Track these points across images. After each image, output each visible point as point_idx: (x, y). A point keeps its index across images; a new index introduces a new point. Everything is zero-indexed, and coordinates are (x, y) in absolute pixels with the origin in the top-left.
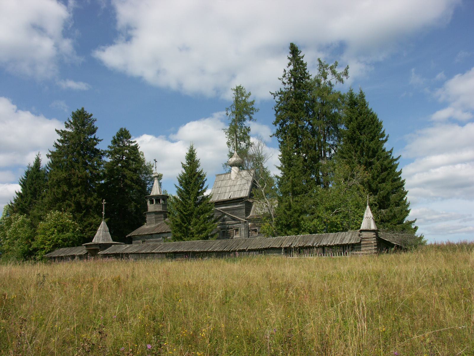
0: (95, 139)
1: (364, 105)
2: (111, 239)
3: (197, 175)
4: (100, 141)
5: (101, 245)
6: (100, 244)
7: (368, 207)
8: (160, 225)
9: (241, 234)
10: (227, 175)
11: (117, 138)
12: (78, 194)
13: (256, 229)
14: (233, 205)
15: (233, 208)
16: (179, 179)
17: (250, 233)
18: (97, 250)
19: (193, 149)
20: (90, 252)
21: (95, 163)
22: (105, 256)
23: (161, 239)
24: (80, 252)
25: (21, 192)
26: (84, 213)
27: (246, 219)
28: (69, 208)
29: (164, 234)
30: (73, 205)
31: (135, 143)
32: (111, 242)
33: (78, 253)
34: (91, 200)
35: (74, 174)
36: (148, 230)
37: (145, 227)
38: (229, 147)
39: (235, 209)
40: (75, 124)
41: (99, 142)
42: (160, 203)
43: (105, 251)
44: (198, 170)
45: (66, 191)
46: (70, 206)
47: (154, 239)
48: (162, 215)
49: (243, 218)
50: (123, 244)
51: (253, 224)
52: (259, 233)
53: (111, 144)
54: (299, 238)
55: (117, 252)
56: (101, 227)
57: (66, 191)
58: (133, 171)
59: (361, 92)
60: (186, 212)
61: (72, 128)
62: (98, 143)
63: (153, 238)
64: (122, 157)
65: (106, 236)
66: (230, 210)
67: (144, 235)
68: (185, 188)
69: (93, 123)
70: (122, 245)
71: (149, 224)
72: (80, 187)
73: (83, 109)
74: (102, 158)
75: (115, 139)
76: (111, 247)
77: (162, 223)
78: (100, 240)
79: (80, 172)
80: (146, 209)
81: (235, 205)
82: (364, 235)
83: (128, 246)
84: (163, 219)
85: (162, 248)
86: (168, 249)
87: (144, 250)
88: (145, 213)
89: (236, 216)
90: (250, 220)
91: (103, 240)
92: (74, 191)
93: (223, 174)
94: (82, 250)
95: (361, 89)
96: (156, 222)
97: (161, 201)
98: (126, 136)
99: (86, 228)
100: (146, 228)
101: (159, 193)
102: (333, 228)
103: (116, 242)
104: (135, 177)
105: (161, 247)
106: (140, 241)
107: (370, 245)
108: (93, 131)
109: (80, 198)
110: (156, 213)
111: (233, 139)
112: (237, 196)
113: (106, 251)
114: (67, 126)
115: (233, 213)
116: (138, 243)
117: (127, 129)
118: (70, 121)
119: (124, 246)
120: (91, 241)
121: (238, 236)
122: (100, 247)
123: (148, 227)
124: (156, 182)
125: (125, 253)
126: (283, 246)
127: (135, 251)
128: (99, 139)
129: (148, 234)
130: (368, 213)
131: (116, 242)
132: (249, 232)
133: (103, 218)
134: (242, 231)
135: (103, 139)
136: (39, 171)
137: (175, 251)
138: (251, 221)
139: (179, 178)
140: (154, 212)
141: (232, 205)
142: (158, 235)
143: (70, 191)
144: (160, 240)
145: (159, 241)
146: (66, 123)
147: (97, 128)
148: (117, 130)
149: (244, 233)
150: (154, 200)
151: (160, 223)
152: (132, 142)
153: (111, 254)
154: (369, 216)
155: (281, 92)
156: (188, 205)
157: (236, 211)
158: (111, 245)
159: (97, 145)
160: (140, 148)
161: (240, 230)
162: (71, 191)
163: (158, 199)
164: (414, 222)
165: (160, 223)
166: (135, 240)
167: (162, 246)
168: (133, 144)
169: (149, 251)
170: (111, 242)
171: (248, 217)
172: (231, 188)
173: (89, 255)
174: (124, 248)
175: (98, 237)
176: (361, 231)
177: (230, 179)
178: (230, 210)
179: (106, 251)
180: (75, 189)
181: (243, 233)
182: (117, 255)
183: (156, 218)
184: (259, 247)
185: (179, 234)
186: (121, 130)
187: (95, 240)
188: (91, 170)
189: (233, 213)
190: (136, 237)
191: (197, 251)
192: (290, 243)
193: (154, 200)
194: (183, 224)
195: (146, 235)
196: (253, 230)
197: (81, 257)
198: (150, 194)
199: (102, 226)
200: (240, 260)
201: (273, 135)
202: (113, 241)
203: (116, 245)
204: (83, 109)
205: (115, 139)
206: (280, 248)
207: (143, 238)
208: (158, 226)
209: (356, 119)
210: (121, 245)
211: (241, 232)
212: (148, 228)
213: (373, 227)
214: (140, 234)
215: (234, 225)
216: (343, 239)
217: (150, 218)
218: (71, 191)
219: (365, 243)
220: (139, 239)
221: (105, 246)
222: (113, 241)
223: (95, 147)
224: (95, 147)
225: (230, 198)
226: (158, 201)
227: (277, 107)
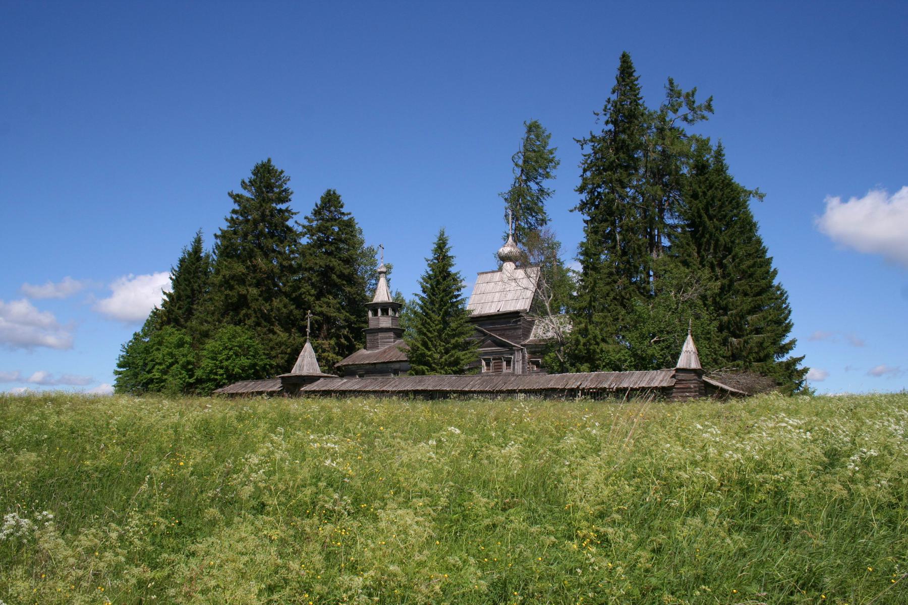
1: (721, 169)
4: (295, 214)
7: (689, 336)
10: (495, 274)
16: (421, 283)
22: (309, 393)
24: (262, 387)
25: (172, 291)
27: (522, 345)
31: (349, 216)
36: (369, 356)
41: (294, 216)
42: (388, 314)
48: (392, 334)
53: (309, 215)
54: (593, 376)
59: (720, 146)
68: (430, 298)
73: (269, 161)
82: (681, 376)
84: (392, 340)
86: (405, 387)
89: (508, 339)
93: (489, 272)
94: (275, 385)
95: (721, 141)
102: (642, 363)
103: (326, 375)
107: (689, 390)
108: (284, 197)
117: (338, 192)
124: (382, 281)
126: (568, 387)
128: (293, 211)
129: (369, 364)
130: (689, 345)
131: (326, 375)
136: (199, 259)
139: (422, 281)
148: (322, 192)
152: (343, 214)
154: (690, 350)
155: (594, 137)
157: (507, 332)
158: (318, 378)
161: (514, 361)
163: (384, 308)
164: (800, 359)
168: (346, 218)
171: (527, 342)
174: (340, 384)
176: (678, 370)
182: (326, 393)
184: (536, 387)
186: (328, 193)
192: (579, 383)
197: (271, 394)
198: (372, 300)
201: (575, 208)
204: (269, 161)
206: (563, 390)
209: (704, 193)
211: (514, 364)
213: (694, 364)
216: (652, 380)
217: (372, 338)
219: (681, 386)
221: (312, 379)
227: (586, 162)
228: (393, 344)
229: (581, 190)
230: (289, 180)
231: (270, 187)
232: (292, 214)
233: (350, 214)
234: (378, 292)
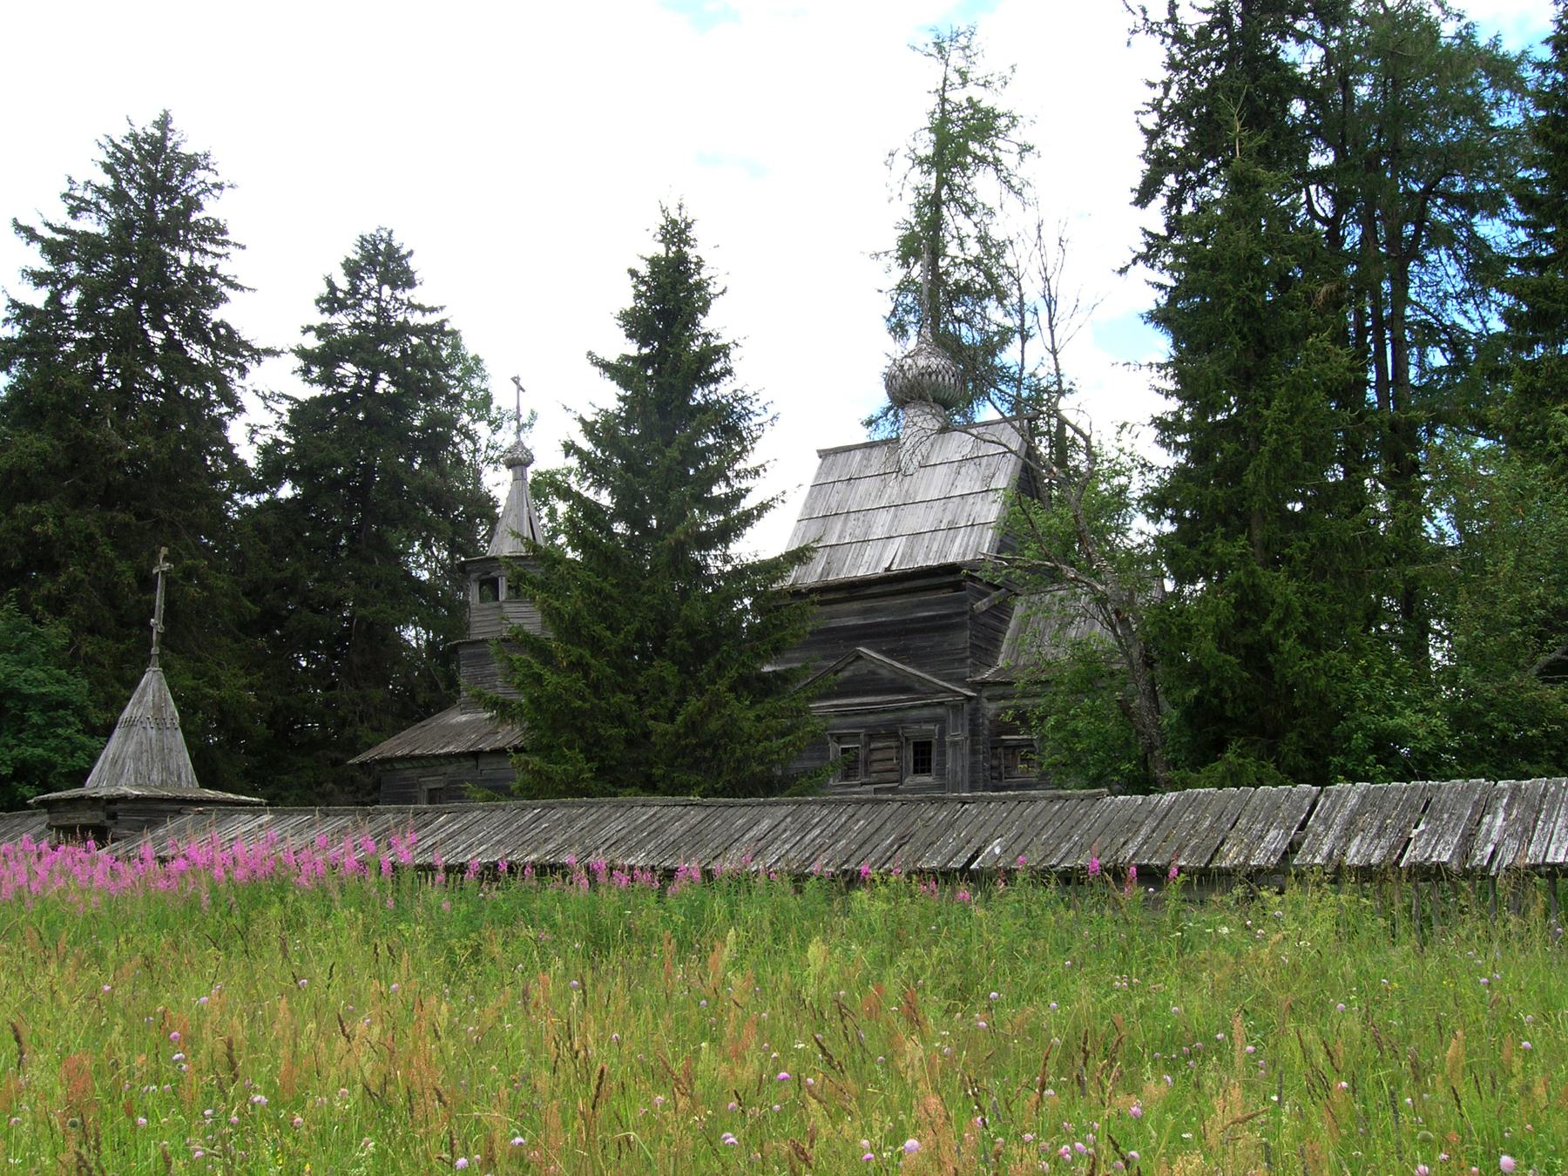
5: (120, 806)
15: (904, 622)
32: (189, 786)
40: (118, 197)
73: (164, 123)
89: (920, 667)
103: (220, 795)
111: (1267, 593)
131: (220, 795)
134: (950, 752)
139: (586, 445)
157: (918, 642)
158: (180, 805)
170: (189, 786)
181: (955, 761)
187: (99, 784)
200: (282, 900)
222: (205, 782)
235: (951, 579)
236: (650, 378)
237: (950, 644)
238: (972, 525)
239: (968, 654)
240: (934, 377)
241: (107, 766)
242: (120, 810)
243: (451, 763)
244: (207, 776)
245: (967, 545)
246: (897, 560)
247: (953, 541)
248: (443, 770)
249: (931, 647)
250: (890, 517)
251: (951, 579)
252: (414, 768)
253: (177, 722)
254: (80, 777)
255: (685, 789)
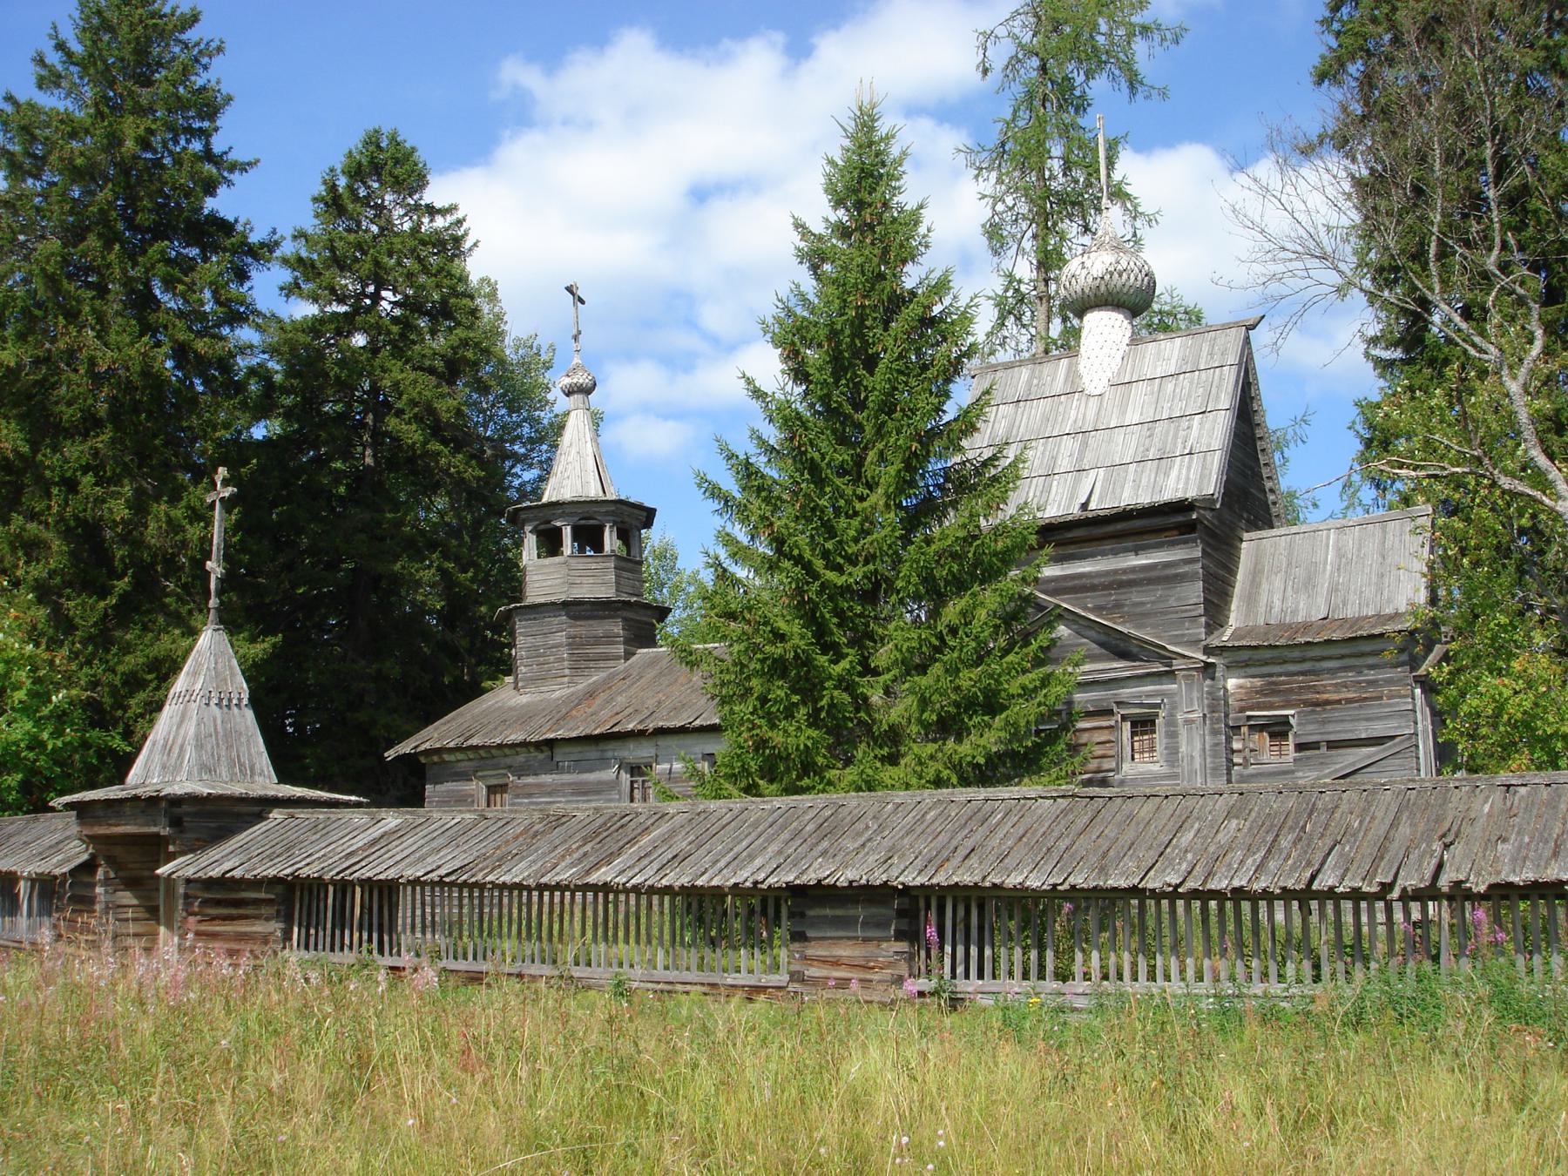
0: (208, 155)
2: (264, 761)
3: (911, 312)
4: (243, 167)
5: (185, 808)
6: (176, 801)
8: (606, 685)
9: (1172, 753)
11: (350, 188)
12: (89, 479)
13: (1284, 722)
14: (1115, 553)
15: (1115, 572)
17: (1236, 745)
18: (156, 849)
19: (872, 129)
20: (112, 861)
21: (207, 294)
23: (609, 774)
26: (124, 597)
27: (1208, 651)
28: (27, 563)
29: (631, 745)
30: (56, 544)
32: (266, 783)
33: (28, 860)
34: (170, 521)
35: (71, 355)
36: (525, 716)
37: (504, 697)
38: (996, 253)
39: (1130, 584)
41: (235, 177)
42: (598, 546)
43: (215, 853)
44: (911, 277)
45: (15, 451)
46: (32, 548)
47: (567, 778)
48: (617, 628)
49: (1194, 643)
50: (358, 805)
51: (1258, 682)
52: (1300, 747)
53: (310, 224)
55: (304, 873)
56: (195, 674)
57: (15, 451)
58: (440, 376)
60: (839, 569)
61: (79, 98)
62: (230, 183)
63: (557, 768)
64: (376, 298)
65: (231, 737)
66: (1093, 588)
67: (500, 746)
69: (206, 68)
70: (346, 814)
71: (533, 680)
72: (107, 436)
74: (253, 273)
75: (333, 188)
76: (261, 827)
77: (611, 677)
78: (177, 768)
79: (106, 345)
80: (511, 581)
81: (1126, 550)
83: (392, 819)
84: (620, 649)
85: (681, 844)
87: (518, 856)
88: (508, 616)
90: (1243, 657)
91: (207, 769)
92: (66, 461)
96: (580, 664)
97: (610, 541)
98: (398, 171)
99: (131, 695)
100: (512, 703)
101: (593, 491)
104: (445, 407)
105: (667, 839)
106: (477, 788)
109: (100, 501)
110: (576, 609)
112: (1136, 492)
113: (223, 860)
114: (49, 80)
115: (1118, 606)
116: (463, 800)
117: (409, 138)
118: (61, 46)
119: (358, 817)
120: (120, 777)
121: (1155, 768)
122: (176, 823)
123: (524, 699)
125: (364, 883)
127: (446, 862)
129: (524, 744)
132: (1229, 740)
133: (213, 602)
135: (258, 161)
137: (810, 878)
138: (1246, 664)
140: (565, 604)
141: (1103, 554)
142: (592, 753)
143: (39, 457)
144: (600, 783)
145: (598, 792)
146: (40, 61)
147: (229, 99)
149: (1198, 746)
150: (567, 533)
151: (603, 675)
152: (432, 211)
153: (257, 883)
156: (856, 523)
157: (1135, 596)
158: (261, 807)
159: (222, 190)
160: (476, 252)
161: (1171, 722)
162: (49, 459)
165: (603, 675)
166: (438, 781)
167: (673, 832)
169: (564, 875)
170: (266, 783)
172: (1085, 444)
173: (106, 882)
174: (360, 841)
175: (167, 749)
177: (1074, 390)
178: (1093, 588)
179: (223, 860)
180: (75, 451)
181: (1190, 741)
183: (574, 643)
185: (795, 735)
186: (373, 141)
188: (181, 337)
189: (1118, 606)
190: (446, 757)
191: (1034, 882)
193: (567, 533)
194: (822, 660)
195: (514, 746)
196: (1260, 728)
199: (198, 665)
202: (282, 780)
203: (302, 814)
205: (333, 188)
207: (496, 767)
208: (591, 694)
210: (335, 814)
211: (1172, 735)
212: (528, 705)
214: (474, 741)
215: (1126, 692)
217: (539, 640)
218: (49, 459)
220: (465, 776)
222: (283, 777)
223: (210, 204)
224: (210, 204)
225: (1084, 506)
226: (589, 537)
228: (622, 665)
229: (1327, 74)
230: (219, 50)
231: (142, 67)
232: (233, 167)
233: (451, 209)
234: (559, 467)
235: (1180, 518)
236: (155, 436)
237: (1179, 599)
238: (1190, 454)
239: (1201, 611)
240: (1125, 276)
241: (157, 758)
242: (188, 814)
243: (517, 754)
244: (286, 765)
245: (1188, 478)
246: (1095, 498)
247: (1167, 474)
248: (508, 761)
249: (1153, 603)
250: (1077, 445)
251: (1180, 518)
252: (470, 760)
253: (245, 696)
254: (121, 765)
255: (1021, 776)
